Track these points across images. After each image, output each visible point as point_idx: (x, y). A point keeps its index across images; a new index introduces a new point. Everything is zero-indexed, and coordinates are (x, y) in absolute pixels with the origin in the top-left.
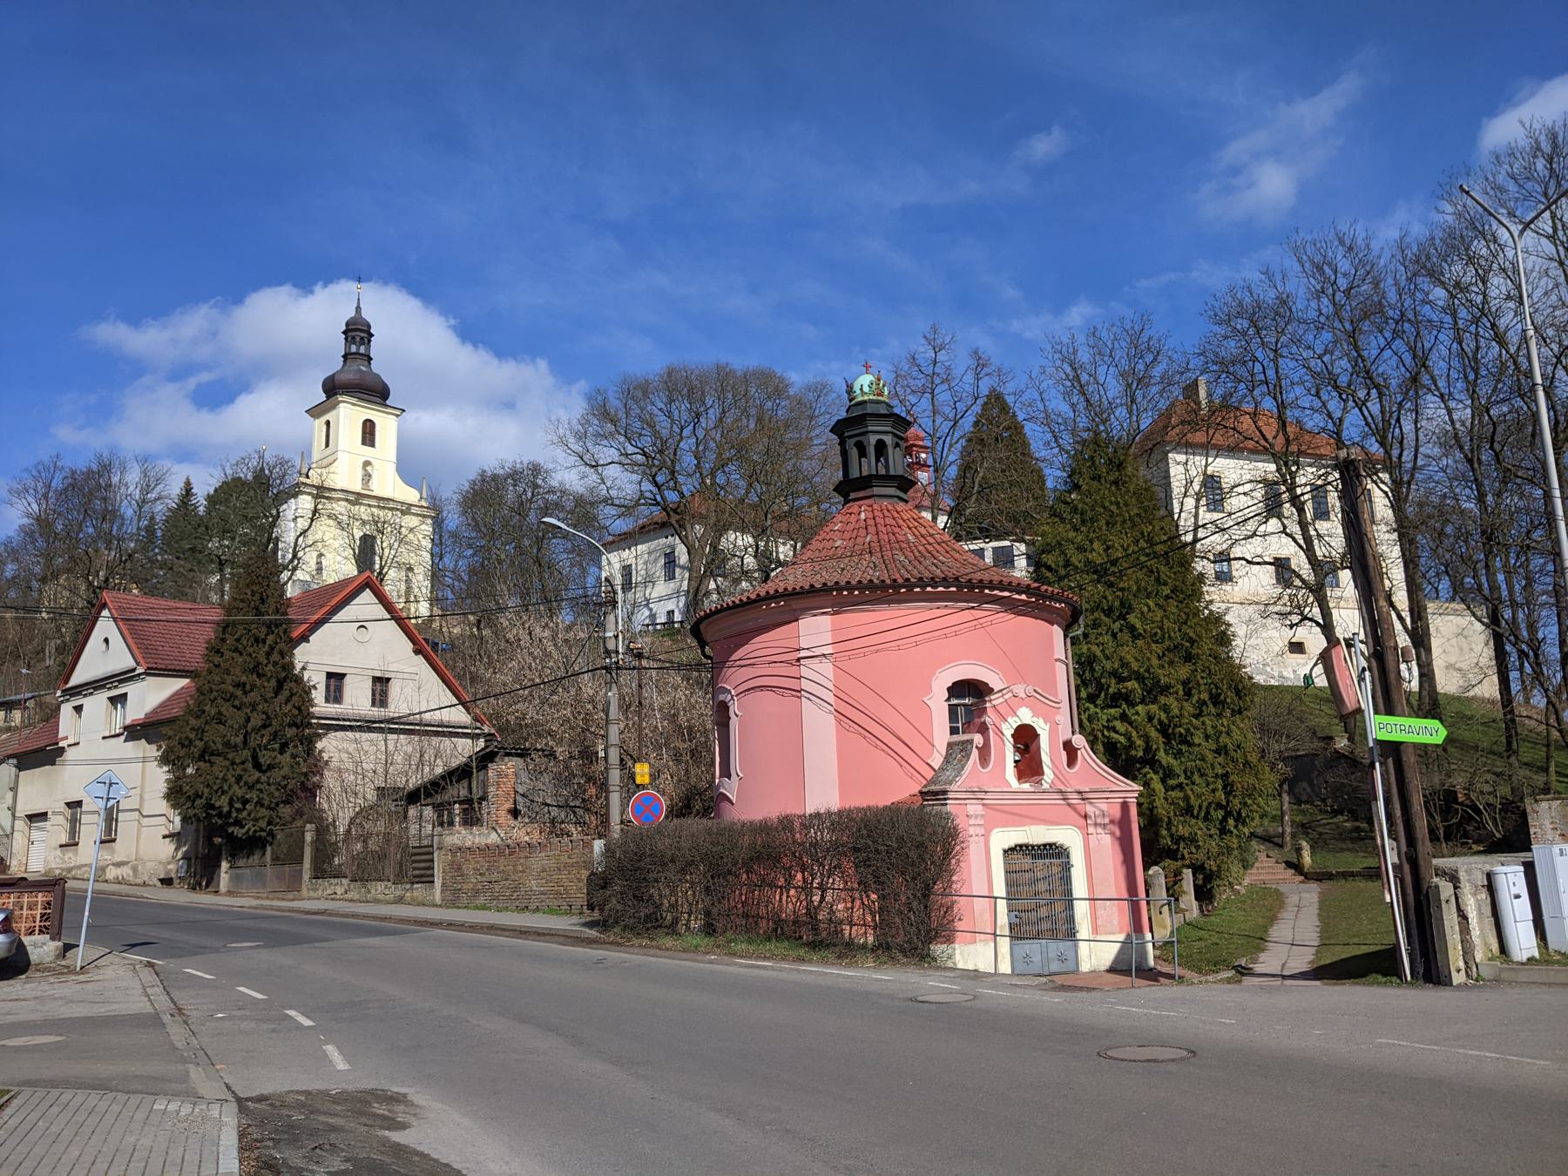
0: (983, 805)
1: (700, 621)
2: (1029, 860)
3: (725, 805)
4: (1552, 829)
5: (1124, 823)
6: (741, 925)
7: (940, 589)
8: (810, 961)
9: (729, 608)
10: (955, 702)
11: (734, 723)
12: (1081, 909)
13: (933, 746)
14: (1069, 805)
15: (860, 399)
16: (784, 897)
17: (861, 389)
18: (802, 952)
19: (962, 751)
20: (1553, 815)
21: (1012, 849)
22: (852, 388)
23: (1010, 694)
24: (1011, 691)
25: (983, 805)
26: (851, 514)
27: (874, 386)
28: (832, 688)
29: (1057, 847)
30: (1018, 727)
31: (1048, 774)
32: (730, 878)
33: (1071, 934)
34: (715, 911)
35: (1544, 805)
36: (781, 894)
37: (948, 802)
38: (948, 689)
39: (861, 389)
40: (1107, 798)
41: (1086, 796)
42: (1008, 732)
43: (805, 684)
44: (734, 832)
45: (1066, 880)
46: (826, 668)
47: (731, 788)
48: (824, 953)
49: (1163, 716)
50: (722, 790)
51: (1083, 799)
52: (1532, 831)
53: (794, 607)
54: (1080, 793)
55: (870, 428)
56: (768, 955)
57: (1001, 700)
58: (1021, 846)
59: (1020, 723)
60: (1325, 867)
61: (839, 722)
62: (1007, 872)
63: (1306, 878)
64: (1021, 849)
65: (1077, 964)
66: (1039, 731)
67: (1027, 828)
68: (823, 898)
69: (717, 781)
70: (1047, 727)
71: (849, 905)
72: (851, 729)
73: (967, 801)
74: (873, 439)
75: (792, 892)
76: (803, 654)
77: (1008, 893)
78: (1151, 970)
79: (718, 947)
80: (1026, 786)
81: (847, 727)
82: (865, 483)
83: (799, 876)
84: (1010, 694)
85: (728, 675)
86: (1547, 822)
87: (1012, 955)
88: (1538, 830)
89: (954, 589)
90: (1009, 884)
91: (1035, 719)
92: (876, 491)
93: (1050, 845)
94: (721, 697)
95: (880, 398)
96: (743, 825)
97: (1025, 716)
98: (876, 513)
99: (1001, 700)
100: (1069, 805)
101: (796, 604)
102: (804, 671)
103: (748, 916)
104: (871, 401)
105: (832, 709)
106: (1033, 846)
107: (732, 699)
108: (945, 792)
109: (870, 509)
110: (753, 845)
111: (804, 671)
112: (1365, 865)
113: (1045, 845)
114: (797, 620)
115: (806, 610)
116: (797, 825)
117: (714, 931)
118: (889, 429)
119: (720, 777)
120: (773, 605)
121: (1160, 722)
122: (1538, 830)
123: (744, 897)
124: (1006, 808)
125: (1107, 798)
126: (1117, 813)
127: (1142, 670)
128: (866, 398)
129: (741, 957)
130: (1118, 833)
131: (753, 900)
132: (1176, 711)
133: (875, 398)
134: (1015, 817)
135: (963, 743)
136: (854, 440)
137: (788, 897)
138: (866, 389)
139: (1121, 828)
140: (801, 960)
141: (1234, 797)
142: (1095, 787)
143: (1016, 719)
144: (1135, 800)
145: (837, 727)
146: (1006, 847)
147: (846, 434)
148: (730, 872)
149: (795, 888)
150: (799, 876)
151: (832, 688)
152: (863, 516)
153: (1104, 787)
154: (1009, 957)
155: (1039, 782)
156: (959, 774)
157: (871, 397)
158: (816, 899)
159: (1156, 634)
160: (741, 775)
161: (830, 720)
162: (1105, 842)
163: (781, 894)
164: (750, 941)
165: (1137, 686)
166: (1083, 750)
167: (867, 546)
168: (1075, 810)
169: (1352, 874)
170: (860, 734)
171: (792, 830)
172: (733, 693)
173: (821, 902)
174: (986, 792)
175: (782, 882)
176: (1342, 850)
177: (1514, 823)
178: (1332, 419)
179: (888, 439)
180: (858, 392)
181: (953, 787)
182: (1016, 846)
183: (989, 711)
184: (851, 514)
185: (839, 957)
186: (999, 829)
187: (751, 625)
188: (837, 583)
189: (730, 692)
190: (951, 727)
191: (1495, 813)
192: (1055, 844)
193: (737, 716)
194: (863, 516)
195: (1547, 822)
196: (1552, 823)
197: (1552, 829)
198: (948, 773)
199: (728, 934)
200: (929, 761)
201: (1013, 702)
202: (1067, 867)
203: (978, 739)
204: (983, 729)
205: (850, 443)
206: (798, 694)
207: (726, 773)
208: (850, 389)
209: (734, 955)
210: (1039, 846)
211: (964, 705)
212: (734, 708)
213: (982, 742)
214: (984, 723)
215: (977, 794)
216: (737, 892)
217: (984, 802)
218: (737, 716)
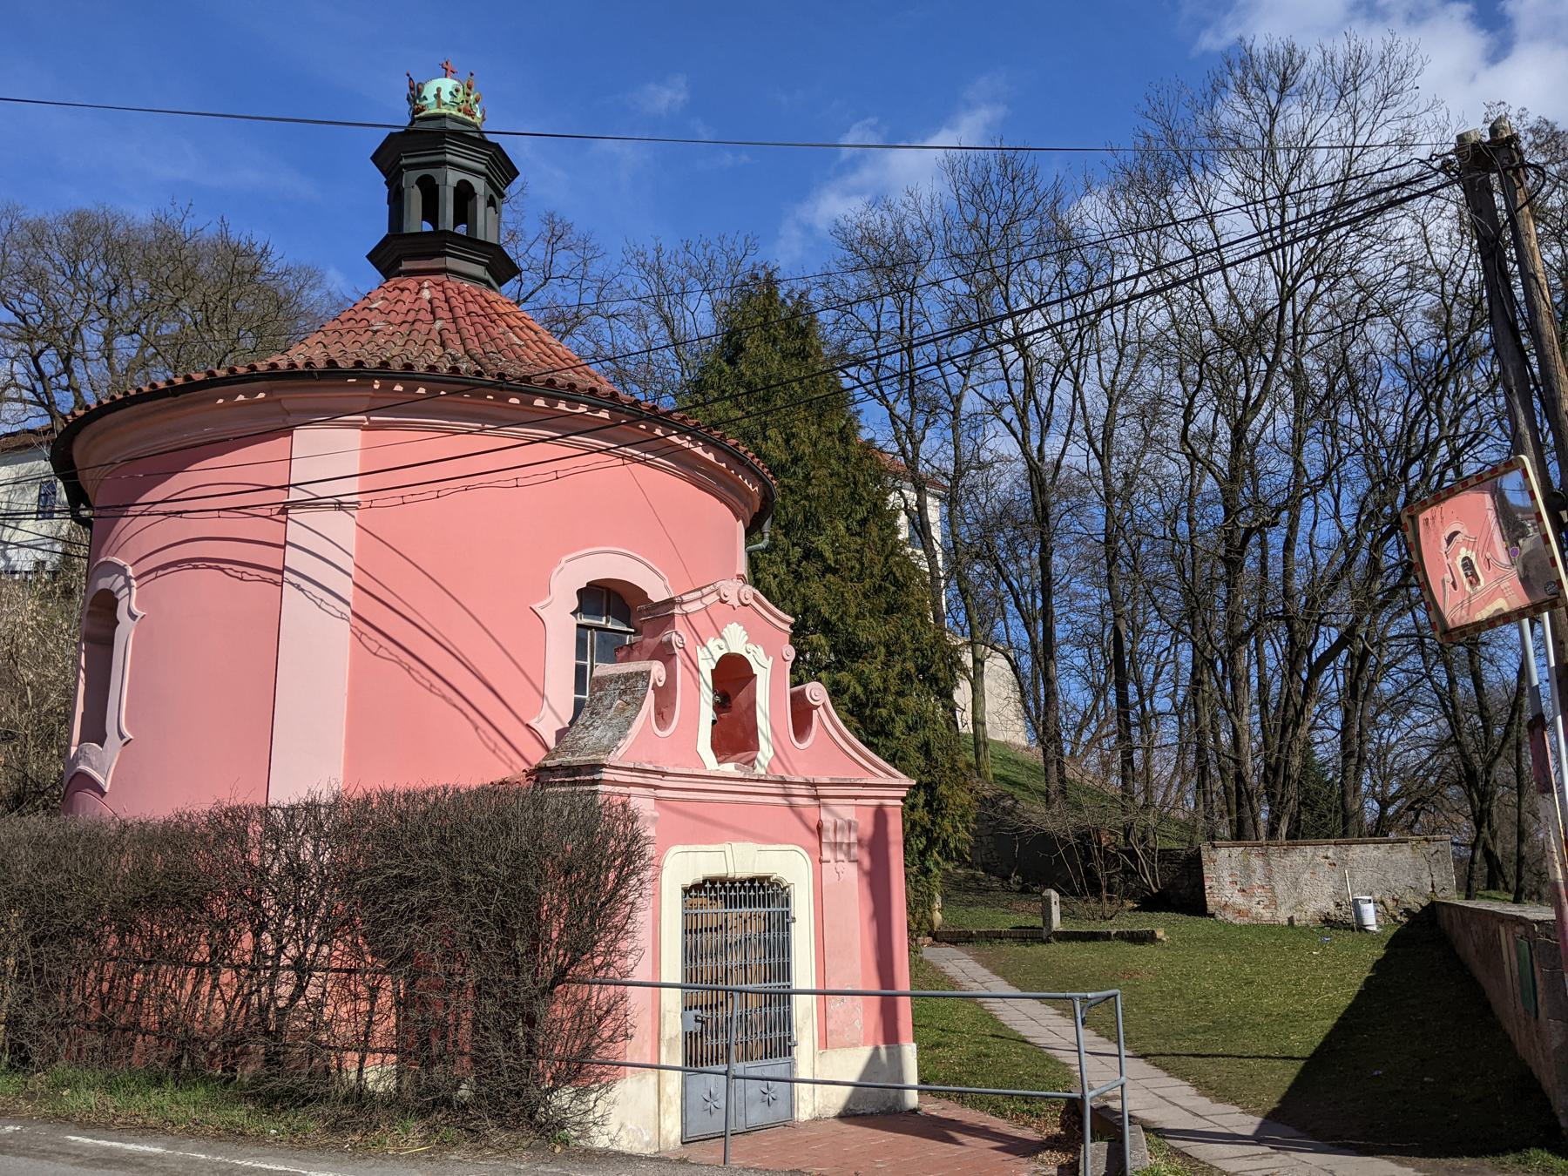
0: (657, 799)
1: (76, 427)
2: (719, 908)
3: (88, 797)
4: (1231, 882)
5: (877, 845)
6: (94, 1050)
7: (582, 409)
8: (260, 1139)
9: (141, 397)
10: (585, 621)
11: (126, 632)
12: (803, 1009)
13: (543, 696)
14: (791, 806)
15: (433, 110)
16: (206, 989)
17: (437, 96)
18: (238, 1115)
19: (624, 692)
20: (1233, 865)
21: (698, 887)
22: (419, 91)
23: (714, 597)
24: (717, 591)
25: (657, 799)
26: (402, 290)
27: (460, 96)
28: (352, 569)
29: (772, 885)
30: (724, 657)
31: (765, 753)
32: (80, 945)
33: (784, 1048)
34: (32, 1016)
35: (1224, 852)
36: (199, 981)
37: (600, 787)
38: (580, 592)
39: (437, 96)
40: (856, 797)
41: (823, 791)
42: (707, 667)
43: (293, 558)
44: (99, 842)
45: (780, 949)
46: (342, 527)
47: (103, 764)
48: (296, 1118)
49: (859, 690)
50: (82, 767)
51: (817, 797)
52: (1207, 884)
53: (287, 405)
54: (814, 785)
55: (449, 157)
56: (152, 1120)
57: (697, 606)
58: (713, 881)
59: (725, 651)
60: (961, 926)
61: (358, 636)
62: (687, 931)
63: (935, 939)
64: (713, 888)
65: (792, 1107)
66: (756, 669)
67: (726, 847)
68: (300, 989)
69: (73, 750)
70: (769, 663)
71: (364, 1006)
72: (382, 652)
73: (632, 790)
74: (453, 177)
75: (226, 976)
76: (295, 495)
77: (688, 974)
78: (914, 1111)
79: (30, 1097)
80: (729, 768)
81: (374, 647)
82: (434, 245)
83: (247, 941)
84: (714, 597)
85: (122, 538)
86: (1225, 874)
87: (684, 1097)
88: (1214, 883)
89: (606, 416)
90: (690, 954)
91: (751, 647)
92: (451, 263)
93: (762, 879)
94: (102, 584)
95: (469, 118)
96: (125, 827)
97: (736, 640)
98: (450, 293)
99: (697, 606)
100: (791, 806)
101: (293, 399)
102: (295, 533)
103: (111, 1028)
104: (455, 119)
105: (347, 610)
106: (733, 882)
107: (128, 584)
108: (596, 767)
109: (440, 288)
110: (143, 872)
111: (295, 533)
112: (1013, 924)
113: (752, 880)
114: (288, 431)
115: (308, 417)
116: (255, 829)
117: (25, 1060)
118: (482, 168)
119: (81, 742)
120: (241, 398)
121: (854, 698)
122: (1214, 883)
123: (105, 986)
124: (681, 805)
125: (856, 797)
126: (867, 827)
127: (834, 617)
128: (444, 111)
129: (85, 1126)
130: (866, 862)
131: (128, 993)
132: (878, 683)
133: (461, 115)
134: (710, 829)
135: (627, 677)
136: (415, 175)
137: (215, 986)
138: (446, 97)
139: (872, 854)
140: (236, 1135)
141: (943, 817)
142: (840, 776)
143: (720, 642)
144: (900, 803)
145: (353, 650)
146: (689, 883)
147: (404, 161)
148: (79, 932)
149: (231, 966)
150: (247, 941)
151: (352, 569)
152: (426, 294)
153: (854, 778)
154: (679, 1102)
155: (751, 762)
156: (622, 734)
157: (454, 112)
158: (285, 990)
159: (853, 567)
160: (129, 735)
161: (342, 632)
162: (848, 877)
163: (199, 981)
164: (110, 1086)
165: (823, 642)
166: (821, 709)
167: (435, 335)
168: (800, 816)
169: (1000, 936)
170: (400, 663)
171: (241, 839)
172: (130, 571)
173: (293, 999)
174: (664, 774)
175: (202, 953)
176: (971, 904)
177: (1171, 875)
178: (949, 393)
179: (479, 185)
180: (431, 99)
181: (613, 759)
182: (705, 881)
183: (678, 621)
184: (402, 290)
185: (336, 1127)
186: (679, 848)
187: (189, 437)
188: (385, 364)
189: (122, 570)
190: (577, 665)
191: (1153, 861)
192: (768, 878)
193: (133, 617)
194: (426, 294)
195: (1225, 874)
196: (1231, 875)
197: (1231, 882)
198: (597, 733)
199: (61, 1064)
200: (532, 723)
201: (719, 612)
202: (785, 922)
203: (657, 670)
204: (665, 654)
205: (410, 178)
206: (278, 578)
207: (95, 732)
208: (415, 93)
209: (66, 1120)
210: (742, 882)
211: (598, 629)
212: (129, 602)
213: (663, 678)
214: (670, 642)
215: (647, 776)
216: (92, 975)
217: (660, 793)
218: (133, 617)
